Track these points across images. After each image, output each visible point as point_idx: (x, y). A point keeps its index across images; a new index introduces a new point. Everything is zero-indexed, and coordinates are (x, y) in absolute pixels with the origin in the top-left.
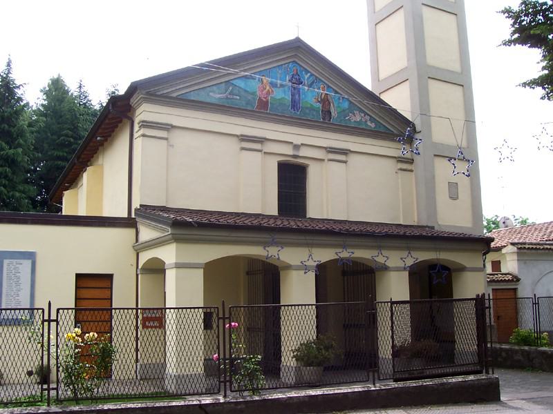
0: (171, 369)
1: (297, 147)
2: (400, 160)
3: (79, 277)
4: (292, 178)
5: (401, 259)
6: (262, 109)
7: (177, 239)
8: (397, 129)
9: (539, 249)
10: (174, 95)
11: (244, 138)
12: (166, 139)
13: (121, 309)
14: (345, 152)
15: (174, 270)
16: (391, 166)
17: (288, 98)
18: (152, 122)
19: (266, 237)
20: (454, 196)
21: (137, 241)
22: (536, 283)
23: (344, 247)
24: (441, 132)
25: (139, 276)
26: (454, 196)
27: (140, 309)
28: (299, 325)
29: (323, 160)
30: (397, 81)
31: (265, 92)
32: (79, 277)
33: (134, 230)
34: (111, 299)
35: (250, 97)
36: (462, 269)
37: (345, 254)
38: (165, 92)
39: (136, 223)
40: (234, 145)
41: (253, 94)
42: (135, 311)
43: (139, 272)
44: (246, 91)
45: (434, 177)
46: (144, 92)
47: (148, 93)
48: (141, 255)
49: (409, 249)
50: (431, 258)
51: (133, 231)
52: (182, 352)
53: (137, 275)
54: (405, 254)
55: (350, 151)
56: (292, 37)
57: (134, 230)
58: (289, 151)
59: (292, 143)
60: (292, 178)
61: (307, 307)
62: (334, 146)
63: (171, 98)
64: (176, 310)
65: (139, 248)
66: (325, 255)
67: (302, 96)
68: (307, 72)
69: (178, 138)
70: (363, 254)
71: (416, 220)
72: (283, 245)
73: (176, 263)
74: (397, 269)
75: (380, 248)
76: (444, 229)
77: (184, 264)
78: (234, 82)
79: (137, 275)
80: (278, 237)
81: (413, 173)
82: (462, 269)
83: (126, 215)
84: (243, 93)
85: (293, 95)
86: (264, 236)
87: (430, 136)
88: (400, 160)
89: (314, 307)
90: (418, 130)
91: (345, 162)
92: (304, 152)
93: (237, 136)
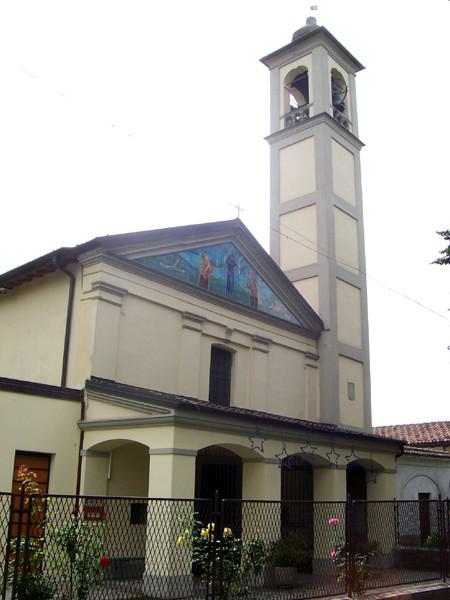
0: (150, 568)
1: (229, 331)
2: (308, 355)
3: (19, 454)
4: (222, 358)
5: (262, 450)
6: (202, 288)
7: (177, 423)
8: (310, 326)
9: (419, 455)
10: (131, 258)
11: (187, 316)
12: (120, 305)
13: (64, 496)
14: (267, 342)
15: (171, 456)
16: (300, 360)
17: (225, 279)
18: (109, 285)
19: (251, 427)
20: (351, 398)
21: (83, 416)
22: (404, 487)
23: (308, 443)
24: (345, 334)
25: (84, 459)
26: (351, 398)
27: (82, 497)
28: (262, 524)
29: (248, 348)
30: (308, 274)
31: (206, 270)
32: (19, 454)
33: (79, 405)
34: (47, 483)
35: (194, 273)
36: (379, 470)
37: (308, 450)
38: (123, 253)
39: (83, 396)
40: (176, 322)
41: (197, 270)
42: (74, 500)
43: (83, 454)
44: (191, 266)
45: (338, 376)
46: (105, 250)
47: (108, 253)
48: (87, 435)
49: (353, 448)
50: (223, 442)
51: (78, 406)
52: (166, 545)
53: (80, 458)
54: (348, 452)
55: (126, 291)
56: (234, 218)
57: (79, 405)
58: (222, 334)
59: (225, 327)
60: (222, 358)
61: (159, 502)
62: (192, 311)
63: (128, 261)
64: (171, 502)
65: (84, 427)
66: (293, 449)
67: (236, 280)
68: (241, 254)
69: (132, 307)
70: (321, 452)
71: (318, 416)
72: (266, 437)
73: (174, 449)
74: (271, 461)
75: (333, 446)
76: (344, 428)
77: (185, 450)
78: (181, 254)
79: (80, 458)
80: (264, 429)
81: (318, 370)
82: (379, 470)
83: (59, 385)
84: (188, 268)
85: (229, 277)
86: (229, 422)
87: (336, 336)
88: (308, 355)
89: (192, 503)
90: (326, 327)
91: (266, 352)
92: (235, 338)
93: (181, 312)
